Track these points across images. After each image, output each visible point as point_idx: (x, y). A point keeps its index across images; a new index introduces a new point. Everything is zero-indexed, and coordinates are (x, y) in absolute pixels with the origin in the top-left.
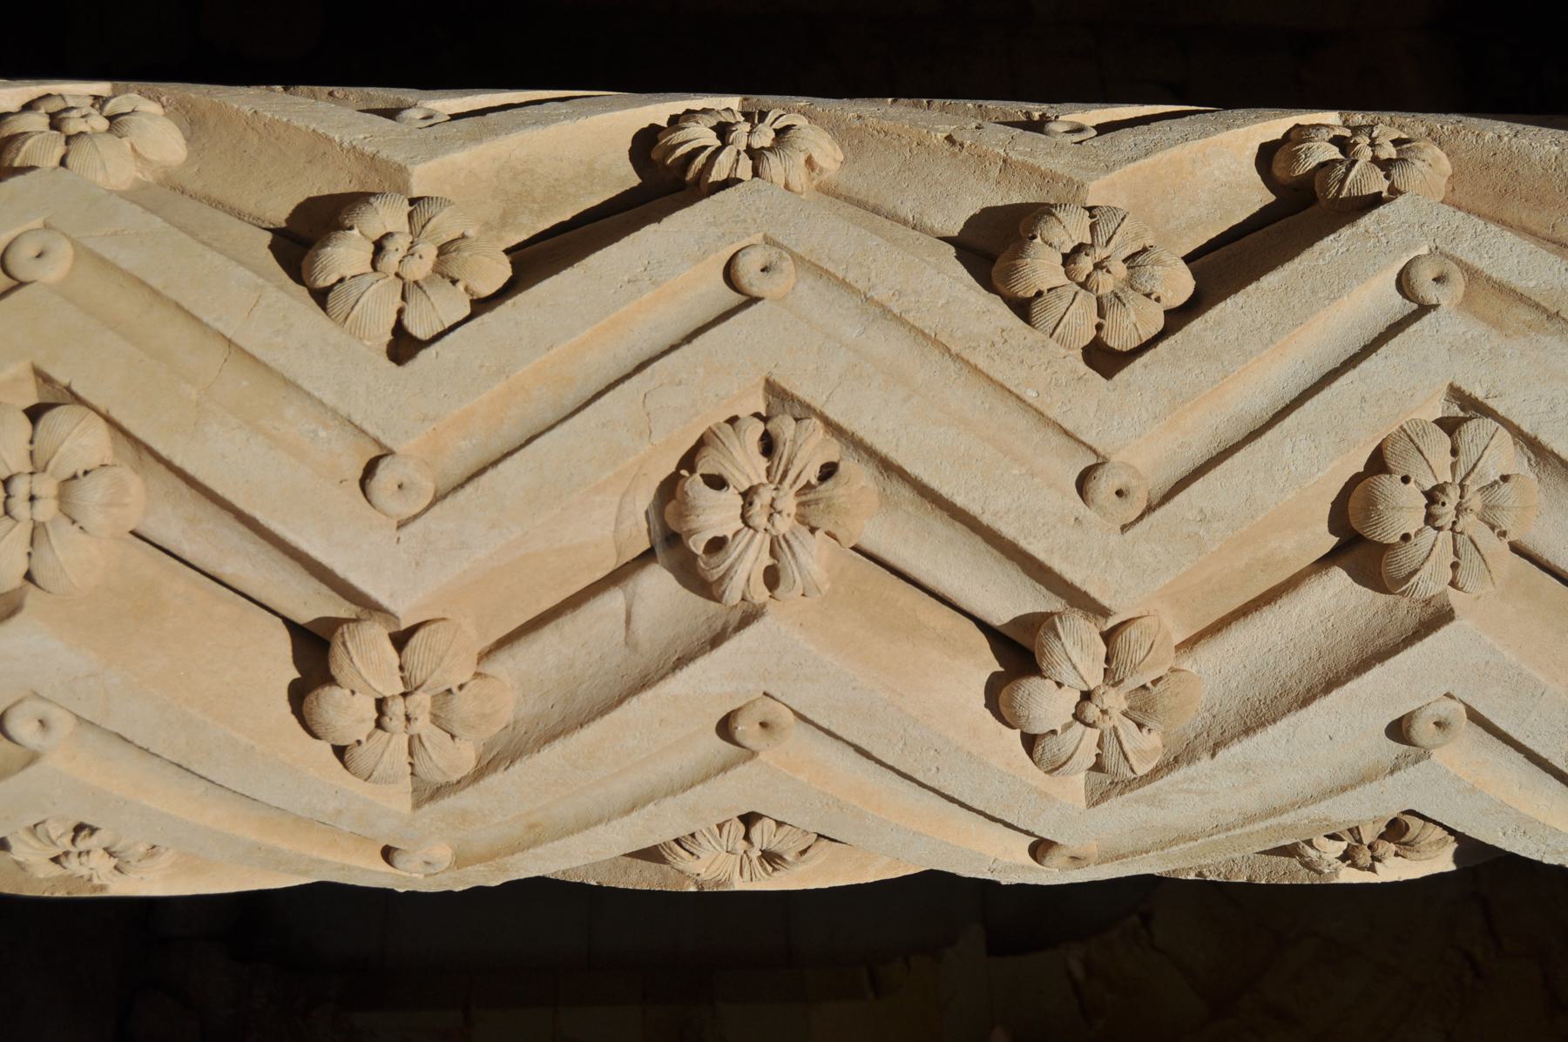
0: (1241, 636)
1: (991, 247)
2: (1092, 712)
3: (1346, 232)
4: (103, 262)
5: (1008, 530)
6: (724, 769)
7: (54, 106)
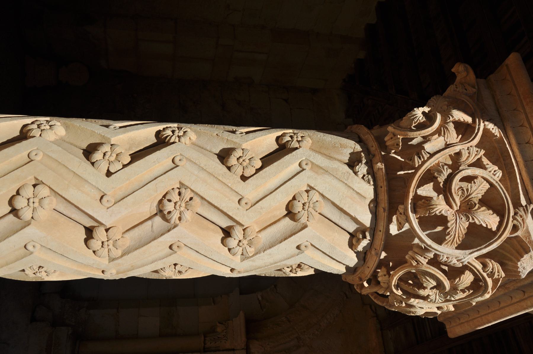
0: (269, 230)
1: (224, 156)
2: (241, 244)
3: (290, 155)
4: (49, 156)
5: (225, 210)
6: (170, 255)
7: (38, 123)
